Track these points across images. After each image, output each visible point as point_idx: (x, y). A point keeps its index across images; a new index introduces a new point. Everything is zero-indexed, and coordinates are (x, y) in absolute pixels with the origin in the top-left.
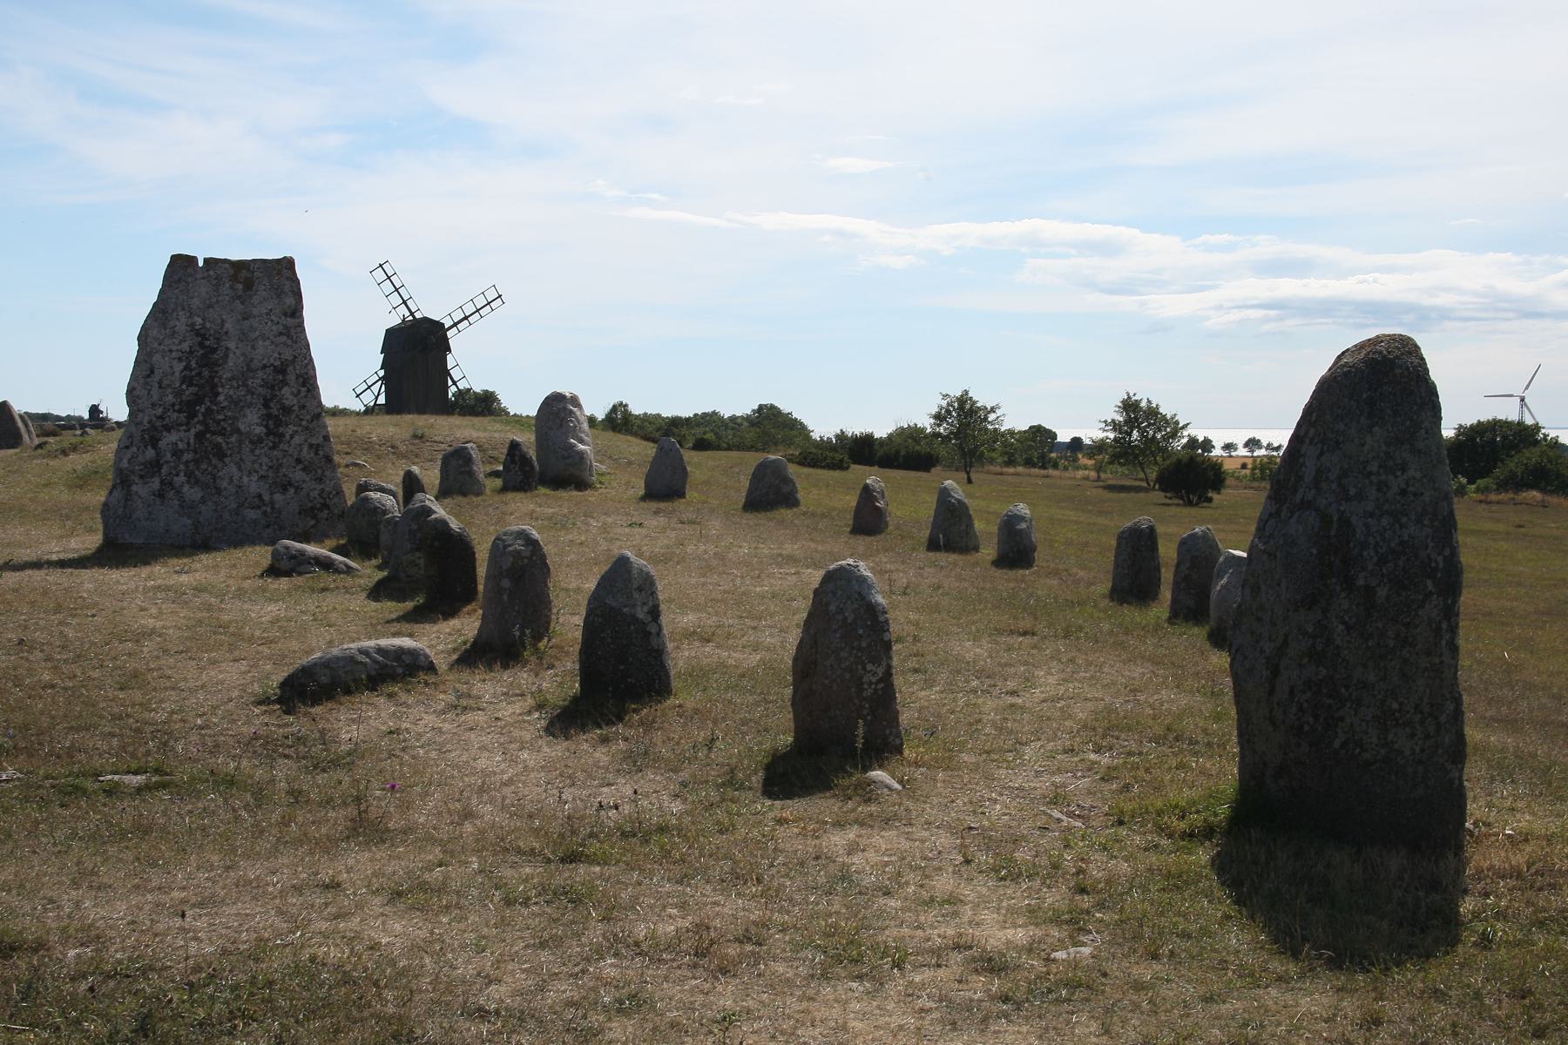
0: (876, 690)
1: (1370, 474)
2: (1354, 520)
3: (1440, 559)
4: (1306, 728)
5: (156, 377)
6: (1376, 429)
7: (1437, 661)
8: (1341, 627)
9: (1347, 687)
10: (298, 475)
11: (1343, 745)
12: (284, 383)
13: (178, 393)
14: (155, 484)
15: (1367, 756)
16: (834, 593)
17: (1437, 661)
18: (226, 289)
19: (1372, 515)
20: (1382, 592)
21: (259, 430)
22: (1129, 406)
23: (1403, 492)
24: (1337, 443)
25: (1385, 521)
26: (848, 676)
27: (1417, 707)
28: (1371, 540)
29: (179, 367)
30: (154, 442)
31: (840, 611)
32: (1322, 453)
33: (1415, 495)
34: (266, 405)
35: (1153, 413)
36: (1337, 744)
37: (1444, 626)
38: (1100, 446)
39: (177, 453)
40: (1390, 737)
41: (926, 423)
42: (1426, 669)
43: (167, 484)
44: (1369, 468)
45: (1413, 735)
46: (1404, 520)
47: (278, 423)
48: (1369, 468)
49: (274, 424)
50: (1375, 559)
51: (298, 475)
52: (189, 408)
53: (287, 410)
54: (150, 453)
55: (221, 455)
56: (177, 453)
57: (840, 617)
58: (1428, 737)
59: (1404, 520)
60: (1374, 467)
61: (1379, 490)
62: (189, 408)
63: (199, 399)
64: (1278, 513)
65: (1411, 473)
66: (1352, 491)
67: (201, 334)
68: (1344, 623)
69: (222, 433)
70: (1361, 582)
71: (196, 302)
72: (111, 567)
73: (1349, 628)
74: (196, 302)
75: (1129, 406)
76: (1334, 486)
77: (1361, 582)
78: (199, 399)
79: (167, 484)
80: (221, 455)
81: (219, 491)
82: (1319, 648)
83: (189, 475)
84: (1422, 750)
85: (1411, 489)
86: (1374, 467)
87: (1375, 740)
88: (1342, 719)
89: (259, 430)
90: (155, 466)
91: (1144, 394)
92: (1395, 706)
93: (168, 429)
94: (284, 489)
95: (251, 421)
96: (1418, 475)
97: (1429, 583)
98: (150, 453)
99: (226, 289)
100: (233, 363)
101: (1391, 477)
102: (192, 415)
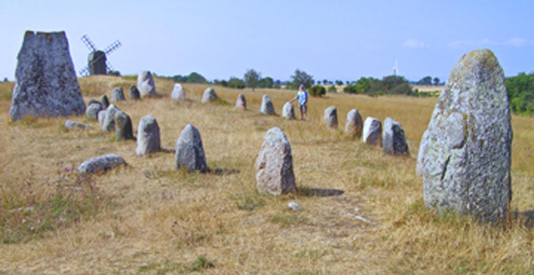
2: (476, 116)
10: (70, 99)
12: (64, 70)
13: (31, 74)
14: (26, 103)
22: (298, 72)
29: (31, 66)
34: (59, 77)
35: (304, 74)
47: (63, 83)
49: (62, 83)
51: (70, 99)
52: (35, 79)
53: (66, 79)
54: (24, 94)
55: (46, 93)
56: (33, 93)
62: (35, 79)
64: (442, 113)
67: (37, 56)
69: (46, 86)
75: (298, 72)
78: (38, 77)
79: (30, 103)
89: (58, 85)
93: (29, 86)
95: (55, 83)
96: (498, 100)
102: (36, 81)
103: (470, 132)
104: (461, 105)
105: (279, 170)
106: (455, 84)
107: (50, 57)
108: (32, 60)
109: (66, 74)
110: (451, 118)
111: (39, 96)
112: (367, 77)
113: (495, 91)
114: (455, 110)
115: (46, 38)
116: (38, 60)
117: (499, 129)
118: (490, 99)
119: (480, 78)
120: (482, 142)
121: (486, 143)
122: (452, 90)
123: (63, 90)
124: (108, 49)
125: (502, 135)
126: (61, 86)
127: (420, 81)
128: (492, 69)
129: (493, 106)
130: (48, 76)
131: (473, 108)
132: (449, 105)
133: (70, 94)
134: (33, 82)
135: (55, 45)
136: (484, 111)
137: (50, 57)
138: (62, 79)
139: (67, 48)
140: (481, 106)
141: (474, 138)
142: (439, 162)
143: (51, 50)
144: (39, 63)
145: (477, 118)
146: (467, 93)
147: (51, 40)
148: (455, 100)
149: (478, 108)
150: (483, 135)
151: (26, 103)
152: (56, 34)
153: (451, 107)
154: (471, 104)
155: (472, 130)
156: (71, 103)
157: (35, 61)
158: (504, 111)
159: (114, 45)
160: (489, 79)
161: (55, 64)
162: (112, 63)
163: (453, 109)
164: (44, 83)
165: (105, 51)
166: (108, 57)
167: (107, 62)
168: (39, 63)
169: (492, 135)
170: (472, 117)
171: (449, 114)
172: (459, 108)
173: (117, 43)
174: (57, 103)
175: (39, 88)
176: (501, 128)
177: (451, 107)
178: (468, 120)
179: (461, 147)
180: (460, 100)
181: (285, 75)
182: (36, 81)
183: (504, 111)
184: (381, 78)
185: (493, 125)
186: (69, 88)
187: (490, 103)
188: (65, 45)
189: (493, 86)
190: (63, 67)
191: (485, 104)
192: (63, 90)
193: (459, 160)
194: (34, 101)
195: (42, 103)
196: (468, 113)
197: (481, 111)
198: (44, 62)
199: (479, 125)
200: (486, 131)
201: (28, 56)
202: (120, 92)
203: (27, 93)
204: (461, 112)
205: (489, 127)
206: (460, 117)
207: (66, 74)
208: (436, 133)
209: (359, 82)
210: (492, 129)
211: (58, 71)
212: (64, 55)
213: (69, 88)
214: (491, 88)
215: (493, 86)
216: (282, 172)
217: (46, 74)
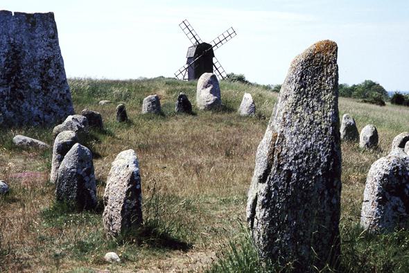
2: (286, 136)
10: (55, 107)
19: (295, 134)
21: (38, 87)
34: (42, 77)
46: (310, 136)
47: (47, 84)
51: (55, 107)
53: (51, 79)
55: (22, 98)
65: (316, 112)
67: (13, 45)
69: (22, 88)
74: (10, 31)
78: (12, 74)
80: (22, 98)
81: (21, 114)
83: (8, 106)
92: (301, 233)
95: (35, 83)
103: (276, 159)
105: (120, 207)
107: (31, 47)
108: (6, 50)
109: (51, 72)
115: (27, 21)
116: (13, 50)
117: (315, 157)
119: (301, 81)
120: (289, 173)
121: (294, 175)
123: (45, 95)
124: (217, 41)
125: (318, 165)
126: (43, 88)
127: (354, 88)
128: (320, 69)
129: (311, 122)
133: (55, 101)
134: (5, 81)
135: (39, 32)
136: (298, 130)
137: (31, 47)
138: (45, 79)
139: (54, 36)
141: (279, 167)
145: (288, 139)
147: (34, 24)
150: (291, 164)
152: (47, 14)
154: (284, 119)
155: (278, 157)
156: (55, 113)
157: (9, 53)
158: (327, 130)
159: (226, 35)
160: (313, 83)
162: (225, 62)
164: (21, 84)
165: (213, 44)
166: (216, 51)
167: (214, 60)
169: (304, 164)
170: (283, 137)
173: (231, 31)
174: (36, 111)
175: (13, 90)
182: (9, 80)
183: (327, 130)
185: (307, 149)
186: (54, 92)
187: (308, 117)
188: (52, 31)
189: (317, 94)
190: (48, 61)
192: (45, 95)
195: (15, 111)
196: (278, 131)
197: (294, 129)
198: (22, 53)
200: (296, 158)
202: (153, 103)
205: (301, 153)
207: (51, 72)
210: (305, 154)
211: (41, 67)
212: (50, 45)
214: (313, 97)
215: (317, 94)
216: (123, 212)
217: (24, 71)
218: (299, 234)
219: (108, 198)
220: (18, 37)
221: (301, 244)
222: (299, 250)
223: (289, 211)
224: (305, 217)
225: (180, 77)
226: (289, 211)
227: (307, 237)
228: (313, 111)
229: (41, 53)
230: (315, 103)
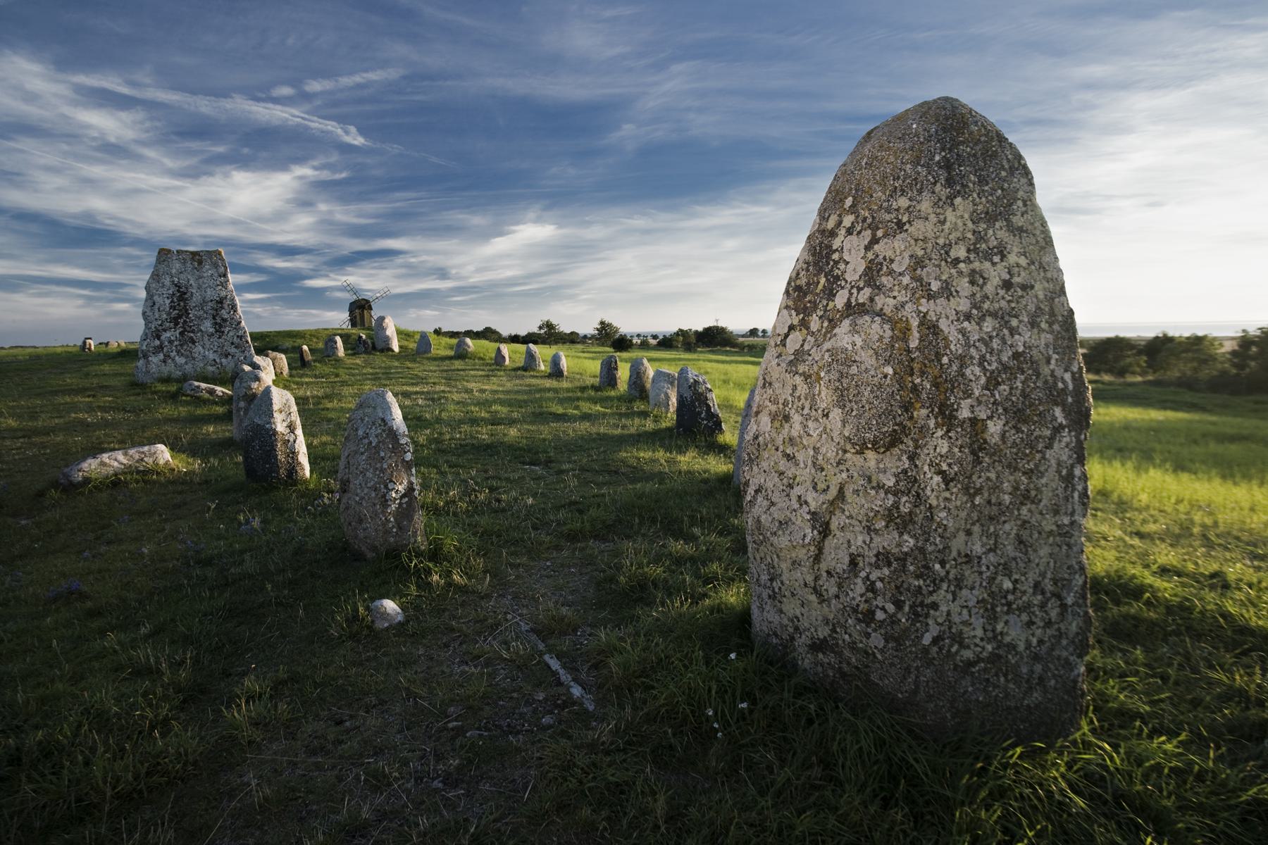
0: (400, 504)
1: (957, 261)
2: (943, 324)
3: (1068, 376)
4: (880, 615)
5: (156, 307)
6: (958, 200)
7: (1066, 521)
8: (937, 479)
9: (943, 563)
10: (233, 350)
11: (936, 640)
12: (222, 308)
13: (169, 314)
14: (161, 356)
15: (968, 654)
16: (362, 420)
17: (1066, 521)
18: (188, 265)
19: (968, 317)
20: (994, 428)
21: (212, 330)
22: (602, 323)
23: (1007, 285)
24: (900, 225)
25: (989, 325)
26: (373, 495)
27: (1037, 586)
28: (973, 351)
29: (168, 302)
30: (158, 337)
31: (367, 435)
32: (875, 240)
33: (1024, 287)
34: (214, 318)
35: (609, 325)
36: (927, 640)
37: (1077, 472)
38: (593, 337)
39: (171, 342)
40: (999, 627)
41: (536, 330)
42: (1051, 533)
43: (167, 356)
44: (953, 254)
45: (1030, 623)
46: (1014, 323)
47: (221, 326)
48: (953, 254)
49: (219, 327)
50: (983, 380)
51: (233, 350)
52: (175, 321)
53: (225, 320)
54: (157, 343)
55: (193, 342)
56: (171, 342)
57: (366, 441)
58: (1049, 624)
59: (1014, 323)
60: (960, 251)
61: (972, 283)
62: (175, 321)
63: (180, 316)
64: (804, 324)
65: (1012, 258)
66: (935, 286)
67: (178, 286)
68: (941, 473)
69: (193, 332)
70: (965, 413)
71: (174, 271)
72: (1157, 338)
73: (947, 480)
74: (174, 271)
75: (602, 323)
76: (906, 280)
77: (965, 413)
78: (180, 316)
79: (167, 356)
80: (193, 342)
81: (194, 359)
82: (905, 509)
83: (178, 352)
84: (1041, 642)
85: (1016, 280)
86: (960, 251)
87: (979, 633)
88: (935, 606)
89: (212, 330)
90: (161, 347)
91: (608, 320)
92: (1007, 585)
93: (165, 331)
94: (226, 356)
95: (207, 326)
96: (1023, 261)
97: (1058, 412)
98: (157, 343)
99: (188, 265)
100: (196, 298)
101: (987, 264)
102: (176, 324)
104: (879, 288)
106: (848, 220)
110: (844, 336)
111: (181, 345)
112: (685, 328)
113: (1011, 229)
114: (852, 310)
115: (193, 259)
118: (996, 259)
122: (836, 244)
130: (195, 315)
131: (931, 297)
132: (831, 295)
135: (208, 271)
138: (218, 321)
140: (964, 285)
142: (802, 502)
143: (201, 277)
144: (181, 295)
146: (899, 243)
147: (200, 263)
148: (854, 266)
149: (947, 291)
151: (161, 356)
153: (840, 301)
161: (208, 299)
163: (848, 304)
168: (181, 295)
170: (930, 328)
171: (833, 324)
172: (871, 300)
176: (1046, 371)
177: (840, 301)
178: (914, 344)
179: (894, 441)
180: (872, 274)
181: (588, 327)
184: (700, 329)
185: (1016, 356)
187: (995, 274)
191: (976, 278)
193: (881, 502)
194: (172, 354)
195: (187, 357)
199: (963, 360)
201: (163, 286)
203: (162, 343)
204: (880, 314)
206: (876, 329)
208: (786, 394)
209: (677, 334)
213: (230, 334)
218: (1001, 589)
219: (348, 481)
220: (182, 276)
221: (1007, 613)
222: (999, 627)
223: (976, 529)
224: (1021, 542)
225: (344, 327)
226: (976, 529)
227: (1024, 593)
228: (1003, 257)
229: (210, 294)
230: (1002, 234)
